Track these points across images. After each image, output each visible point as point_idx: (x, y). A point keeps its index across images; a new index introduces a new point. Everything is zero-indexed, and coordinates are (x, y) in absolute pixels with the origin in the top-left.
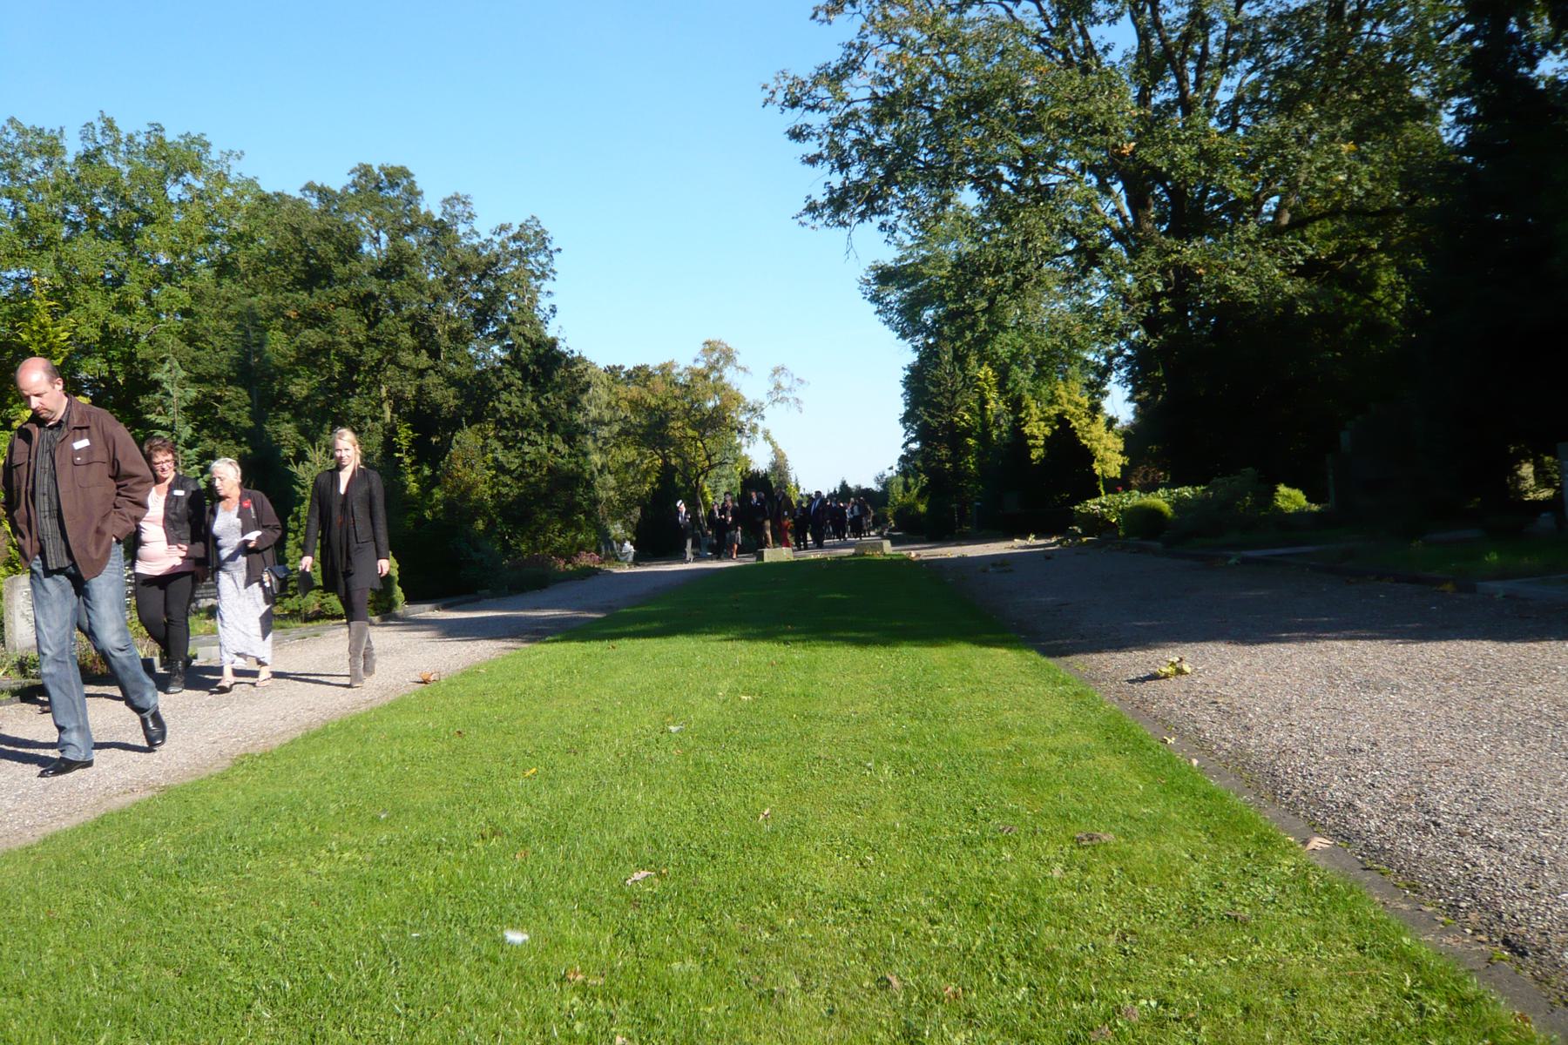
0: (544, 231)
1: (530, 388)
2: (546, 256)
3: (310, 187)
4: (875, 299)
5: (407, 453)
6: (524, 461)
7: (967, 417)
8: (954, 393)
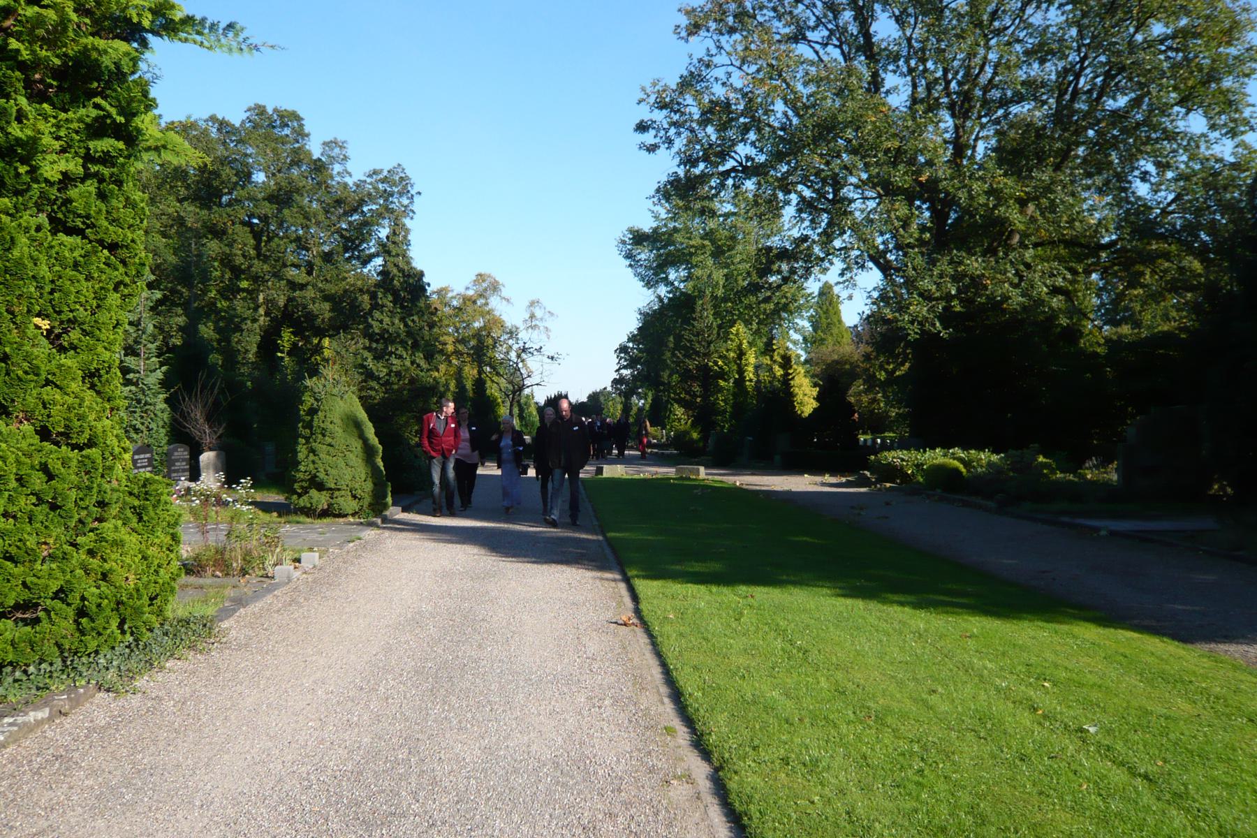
0: (408, 178)
1: (399, 310)
2: (408, 198)
3: (213, 118)
4: (629, 256)
5: (288, 354)
6: (391, 371)
7: (720, 363)
8: (709, 343)
